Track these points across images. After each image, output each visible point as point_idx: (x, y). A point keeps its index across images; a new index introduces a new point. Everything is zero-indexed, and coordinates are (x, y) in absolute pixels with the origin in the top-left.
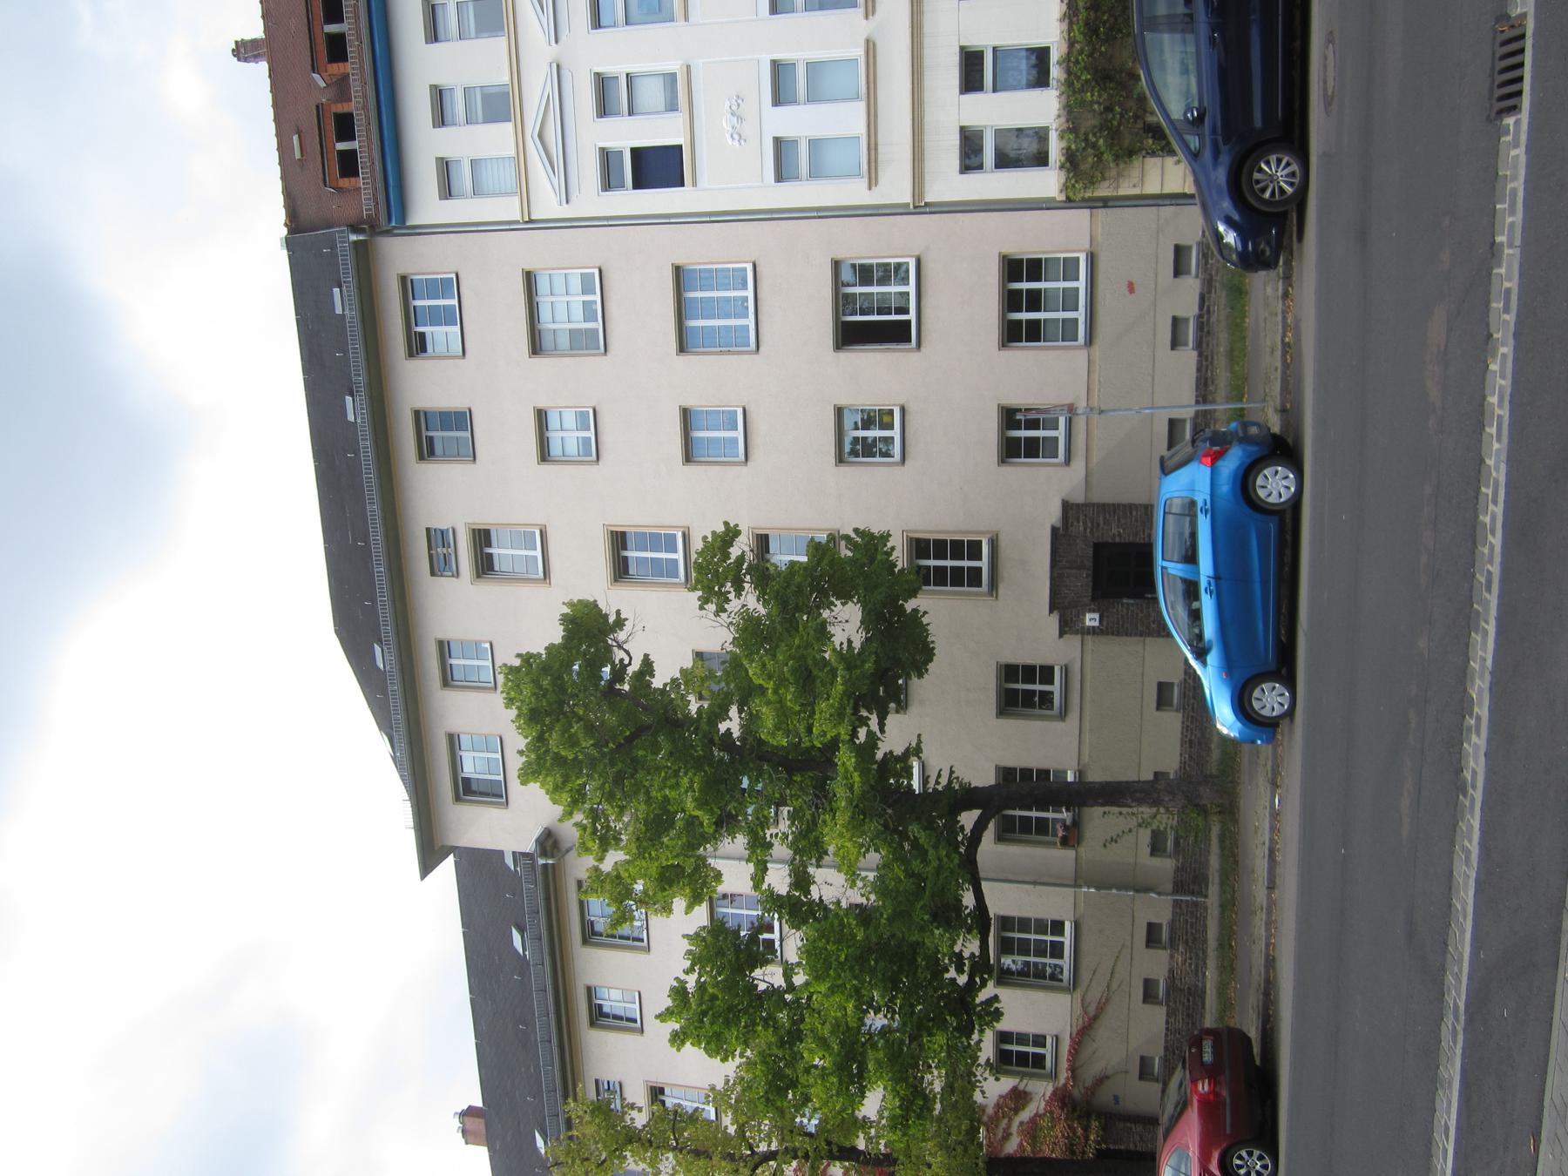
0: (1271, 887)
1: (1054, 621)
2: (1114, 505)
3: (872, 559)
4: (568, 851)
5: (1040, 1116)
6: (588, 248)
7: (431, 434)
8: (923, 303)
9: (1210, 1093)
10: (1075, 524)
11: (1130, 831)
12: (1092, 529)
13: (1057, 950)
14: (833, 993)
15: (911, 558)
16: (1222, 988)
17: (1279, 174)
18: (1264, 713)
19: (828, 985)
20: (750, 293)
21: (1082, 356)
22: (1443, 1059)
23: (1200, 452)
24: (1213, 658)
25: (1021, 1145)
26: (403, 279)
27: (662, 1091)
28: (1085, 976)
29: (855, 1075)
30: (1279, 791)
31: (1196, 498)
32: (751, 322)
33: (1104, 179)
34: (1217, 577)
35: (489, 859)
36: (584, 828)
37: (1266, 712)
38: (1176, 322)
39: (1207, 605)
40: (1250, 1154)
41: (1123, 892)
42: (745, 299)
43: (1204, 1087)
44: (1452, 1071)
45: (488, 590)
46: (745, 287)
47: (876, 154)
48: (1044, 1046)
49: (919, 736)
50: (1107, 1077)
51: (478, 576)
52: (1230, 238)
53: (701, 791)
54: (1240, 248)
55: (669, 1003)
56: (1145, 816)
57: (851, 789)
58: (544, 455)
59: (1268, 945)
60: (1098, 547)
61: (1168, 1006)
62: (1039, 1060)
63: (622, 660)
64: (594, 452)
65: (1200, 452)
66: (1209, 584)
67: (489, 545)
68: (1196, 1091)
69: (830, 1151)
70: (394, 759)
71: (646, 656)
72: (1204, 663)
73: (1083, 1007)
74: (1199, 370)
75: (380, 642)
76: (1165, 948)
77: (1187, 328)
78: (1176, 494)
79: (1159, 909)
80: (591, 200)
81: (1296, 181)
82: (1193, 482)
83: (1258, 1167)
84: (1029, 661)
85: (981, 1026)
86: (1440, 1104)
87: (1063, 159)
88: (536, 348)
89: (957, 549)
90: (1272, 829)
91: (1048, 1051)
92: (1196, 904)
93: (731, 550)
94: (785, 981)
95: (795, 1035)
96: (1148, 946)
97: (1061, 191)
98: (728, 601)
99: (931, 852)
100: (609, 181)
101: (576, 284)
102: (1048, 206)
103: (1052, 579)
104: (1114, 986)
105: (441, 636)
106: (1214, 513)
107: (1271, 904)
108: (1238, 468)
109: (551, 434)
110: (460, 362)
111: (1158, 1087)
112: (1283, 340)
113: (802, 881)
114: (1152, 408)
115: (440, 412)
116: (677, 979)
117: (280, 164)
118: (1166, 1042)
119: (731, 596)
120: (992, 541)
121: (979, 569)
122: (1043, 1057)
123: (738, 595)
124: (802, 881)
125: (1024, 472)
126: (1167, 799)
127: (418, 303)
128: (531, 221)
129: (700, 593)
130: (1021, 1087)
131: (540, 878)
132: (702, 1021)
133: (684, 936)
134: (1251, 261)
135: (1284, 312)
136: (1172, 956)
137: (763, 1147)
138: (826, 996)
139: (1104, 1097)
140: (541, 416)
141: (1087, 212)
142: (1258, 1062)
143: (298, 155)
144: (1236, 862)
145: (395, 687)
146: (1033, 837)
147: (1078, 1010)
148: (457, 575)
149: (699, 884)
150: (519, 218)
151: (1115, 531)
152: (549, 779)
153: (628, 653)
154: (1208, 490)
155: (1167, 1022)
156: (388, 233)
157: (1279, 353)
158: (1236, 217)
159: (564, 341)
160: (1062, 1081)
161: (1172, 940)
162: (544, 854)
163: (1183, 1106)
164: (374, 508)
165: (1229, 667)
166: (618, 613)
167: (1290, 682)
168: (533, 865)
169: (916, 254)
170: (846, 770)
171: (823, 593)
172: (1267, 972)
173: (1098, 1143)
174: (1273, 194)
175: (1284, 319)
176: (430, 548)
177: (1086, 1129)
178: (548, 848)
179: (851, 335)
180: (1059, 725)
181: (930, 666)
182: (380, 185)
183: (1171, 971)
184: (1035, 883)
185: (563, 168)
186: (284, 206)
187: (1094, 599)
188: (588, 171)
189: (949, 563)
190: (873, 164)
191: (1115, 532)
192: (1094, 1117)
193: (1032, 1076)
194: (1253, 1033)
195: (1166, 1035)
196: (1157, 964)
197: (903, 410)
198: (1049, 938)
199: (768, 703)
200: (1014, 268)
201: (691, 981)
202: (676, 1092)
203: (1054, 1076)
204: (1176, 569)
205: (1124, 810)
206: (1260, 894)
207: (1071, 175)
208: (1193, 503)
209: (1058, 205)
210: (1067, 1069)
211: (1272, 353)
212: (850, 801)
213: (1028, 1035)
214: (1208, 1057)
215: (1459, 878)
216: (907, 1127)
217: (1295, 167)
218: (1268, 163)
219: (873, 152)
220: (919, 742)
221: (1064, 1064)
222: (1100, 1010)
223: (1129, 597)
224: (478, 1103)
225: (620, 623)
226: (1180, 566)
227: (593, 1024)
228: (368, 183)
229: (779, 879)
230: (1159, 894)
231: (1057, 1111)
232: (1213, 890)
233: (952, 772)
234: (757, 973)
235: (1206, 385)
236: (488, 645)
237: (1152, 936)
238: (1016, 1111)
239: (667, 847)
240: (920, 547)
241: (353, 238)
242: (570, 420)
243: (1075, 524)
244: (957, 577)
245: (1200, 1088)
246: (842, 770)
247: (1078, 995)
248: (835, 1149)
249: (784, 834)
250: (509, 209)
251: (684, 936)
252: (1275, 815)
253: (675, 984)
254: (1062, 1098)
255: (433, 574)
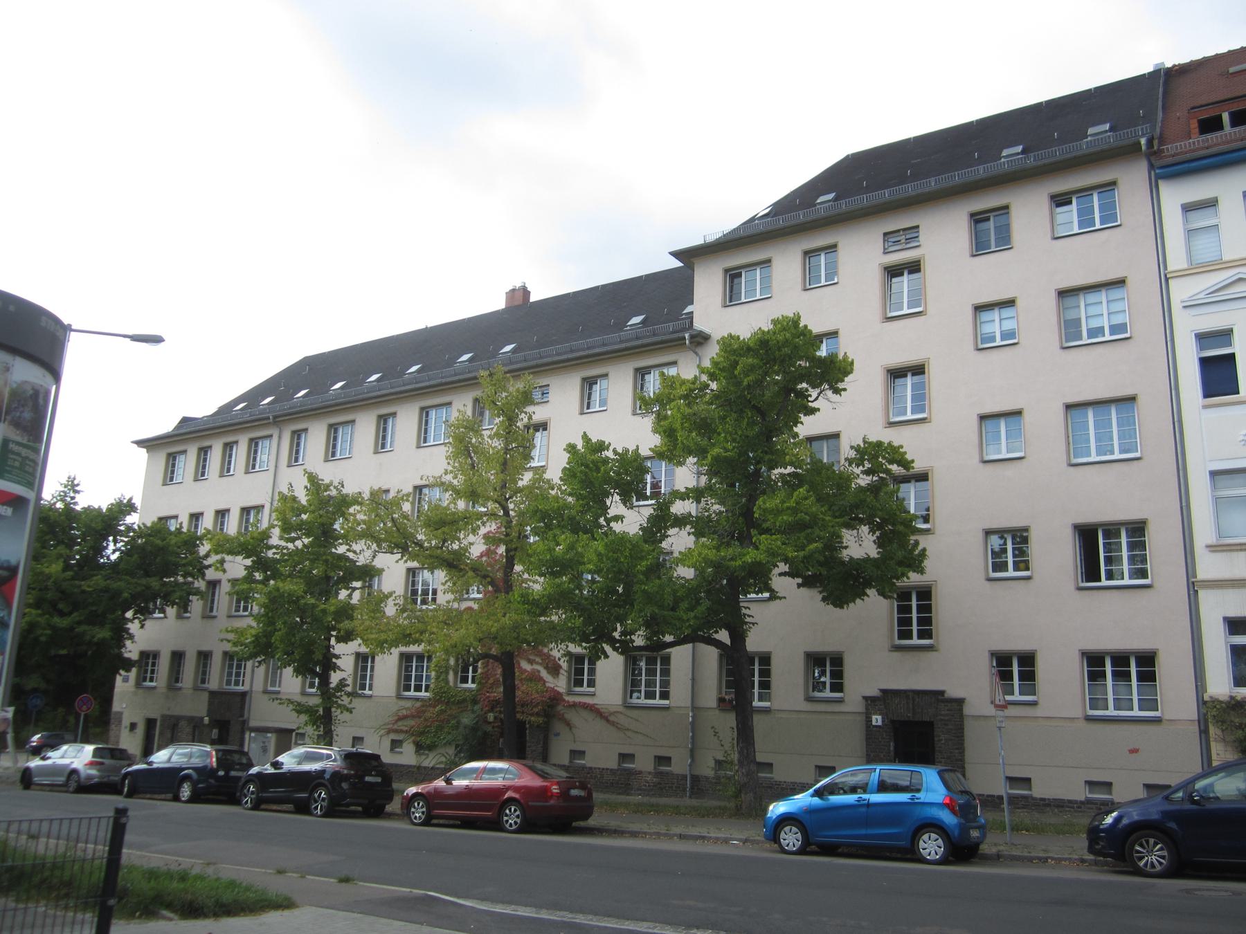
0: (681, 837)
1: (873, 692)
2: (963, 736)
3: (900, 563)
4: (696, 353)
5: (544, 684)
6: (1147, 328)
7: (992, 219)
8: (1114, 591)
9: (552, 793)
10: (946, 708)
11: (722, 746)
12: (942, 720)
13: (651, 695)
14: (598, 555)
15: (915, 588)
16: (626, 805)
17: (1153, 857)
18: (782, 833)
19: (603, 552)
20: (1117, 456)
21: (1078, 713)
22: (550, 912)
23: (955, 797)
24: (816, 800)
25: (525, 671)
26: (1113, 183)
27: (545, 429)
28: (629, 712)
29: (552, 570)
30: (741, 844)
31: (922, 792)
32: (1094, 458)
33: (1223, 731)
34: (869, 805)
35: (687, 296)
36: (694, 383)
37: (782, 835)
38: (1027, 781)
39: (850, 798)
40: (518, 817)
41: (690, 740)
42: (1112, 453)
43: (555, 789)
44: (544, 915)
45: (874, 277)
46: (1121, 452)
47: (1237, 550)
48: (588, 686)
49: (785, 598)
50: (570, 729)
51: (885, 268)
52: (1109, 820)
53: (726, 457)
54: (1101, 827)
55: (594, 440)
56: (732, 756)
57: (732, 559)
58: (979, 308)
59: (645, 833)
60: (930, 724)
61: (618, 770)
62: (579, 683)
63: (810, 396)
64: (983, 345)
65: (955, 797)
66: (864, 800)
67: (910, 272)
68: (552, 785)
69: (511, 550)
70: (753, 219)
71: (818, 410)
72: (813, 796)
73: (615, 712)
74: (1070, 801)
75: (835, 199)
76: (655, 768)
77: (1104, 794)
78: (924, 779)
79: (679, 766)
80: (1187, 326)
81: (1148, 869)
82: (933, 791)
83: (510, 821)
84: (846, 675)
85: (589, 647)
86: (528, 909)
87: (1239, 698)
88: (1063, 294)
89: (926, 621)
90: (717, 839)
91: (585, 689)
92: (684, 790)
93: (895, 465)
94: (612, 517)
95: (576, 528)
96: (655, 757)
97: (1211, 697)
98: (858, 466)
99: (692, 614)
100: (1203, 338)
101: (1117, 320)
102: (1199, 688)
103: (905, 692)
104: (629, 733)
105: (840, 246)
106: (912, 804)
107: (670, 837)
108: (943, 822)
109: (996, 312)
110: (1049, 235)
111: (566, 762)
112: (1049, 857)
113: (680, 521)
114: (1004, 764)
115: (1009, 225)
116: (610, 444)
117: (1229, 51)
118: (595, 768)
119: (861, 468)
120: (932, 647)
121: (911, 638)
122: (582, 685)
123: (864, 472)
124: (680, 521)
125: (984, 670)
126: (744, 771)
127: (1095, 197)
128: (1167, 280)
129: (862, 446)
130: (562, 671)
131: (676, 335)
132: (582, 465)
133: (637, 446)
134: (1094, 834)
135: (1070, 859)
136: (650, 773)
137: (511, 506)
138: (596, 550)
139: (558, 726)
140: (1010, 303)
141: (1196, 717)
142: (574, 824)
143: (1232, 70)
144: (703, 816)
145: (801, 216)
146: (724, 679)
147: (612, 709)
148: (885, 253)
149: (671, 453)
150: (1170, 268)
151: (943, 737)
152: (722, 359)
153: (816, 399)
154: (927, 801)
155: (607, 769)
156: (1151, 167)
157: (1042, 855)
158: (1120, 826)
159: (1071, 315)
160: (567, 698)
161: (661, 773)
162: (692, 337)
163: (543, 775)
164: (932, 184)
165: (811, 811)
166: (845, 390)
167: (802, 851)
168: (684, 330)
169: (1155, 585)
170: (745, 555)
171: (880, 527)
172: (629, 832)
173: (529, 722)
174: (1138, 852)
175: (1065, 859)
176: (904, 230)
177: (538, 714)
178: (696, 339)
179: (1087, 535)
180: (801, 696)
181: (831, 606)
182: (1188, 156)
183: (640, 772)
184: (693, 679)
185: (1215, 298)
186: (1192, 61)
187: (893, 722)
188: (1212, 321)
189: (914, 615)
190: (1228, 548)
191: (942, 738)
192: (546, 720)
193: (569, 678)
194: (592, 822)
195: (599, 768)
196: (643, 763)
197: (1029, 578)
198: (658, 689)
199: (783, 502)
200: (1147, 660)
201: (609, 454)
202: (545, 439)
203: (570, 693)
204: (874, 778)
205: (735, 742)
206: (677, 830)
207: (1224, 705)
208: (918, 791)
209: (1200, 694)
210: (574, 702)
211: (1043, 850)
212: (724, 558)
213: (595, 675)
214: (574, 792)
215: (641, 924)
216: (524, 603)
217: (1158, 868)
218: (1161, 849)
219: (1239, 548)
220: (780, 598)
221: (577, 699)
222: (613, 724)
223: (895, 748)
224: (533, 298)
225: (837, 391)
226: (876, 782)
227: (584, 380)
228: (1190, 146)
229: (679, 508)
230: (690, 765)
231: (547, 695)
232: (694, 802)
233: (753, 624)
234: (616, 498)
235: (1058, 806)
236: (836, 281)
237: (663, 760)
238: (546, 668)
239: (689, 436)
240: (925, 594)
241: (1143, 141)
242: (1009, 325)
243: (946, 708)
244: (904, 622)
245: (554, 787)
246: (745, 552)
247: (621, 709)
248: (512, 553)
249: (709, 509)
250: (1176, 260)
251: (637, 446)
252: (726, 841)
253: (606, 443)
254: (556, 698)
255: (885, 234)
